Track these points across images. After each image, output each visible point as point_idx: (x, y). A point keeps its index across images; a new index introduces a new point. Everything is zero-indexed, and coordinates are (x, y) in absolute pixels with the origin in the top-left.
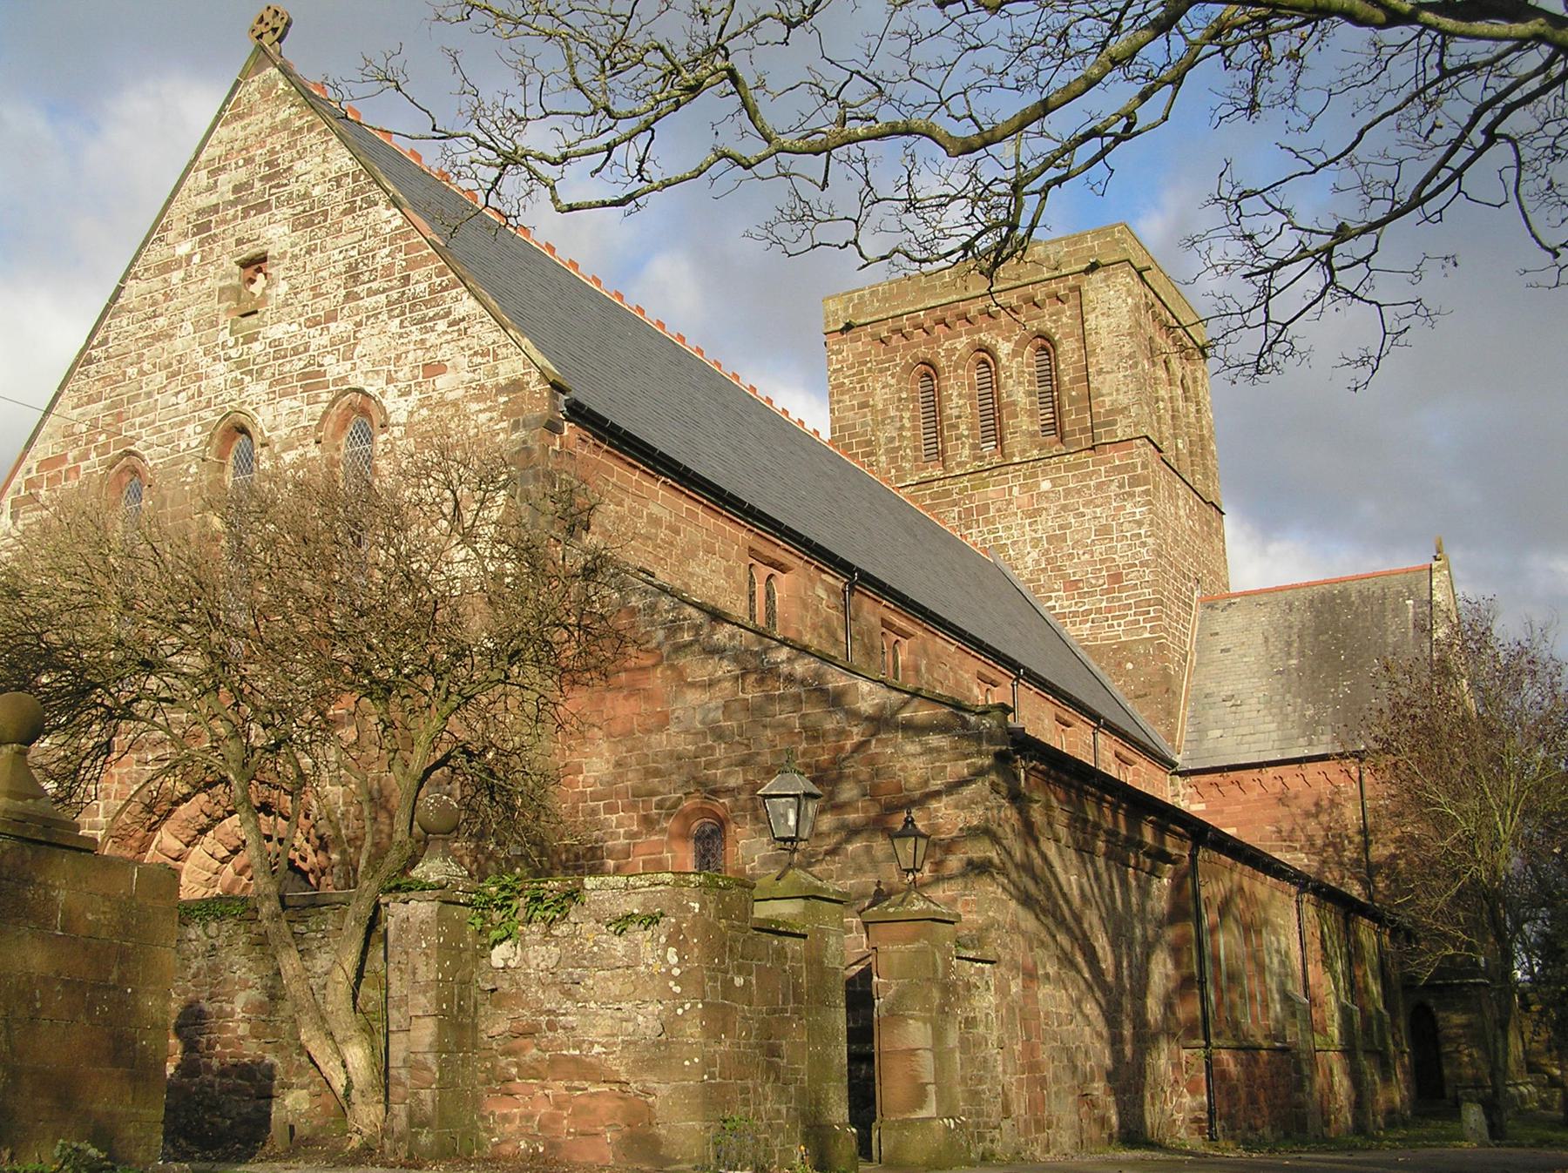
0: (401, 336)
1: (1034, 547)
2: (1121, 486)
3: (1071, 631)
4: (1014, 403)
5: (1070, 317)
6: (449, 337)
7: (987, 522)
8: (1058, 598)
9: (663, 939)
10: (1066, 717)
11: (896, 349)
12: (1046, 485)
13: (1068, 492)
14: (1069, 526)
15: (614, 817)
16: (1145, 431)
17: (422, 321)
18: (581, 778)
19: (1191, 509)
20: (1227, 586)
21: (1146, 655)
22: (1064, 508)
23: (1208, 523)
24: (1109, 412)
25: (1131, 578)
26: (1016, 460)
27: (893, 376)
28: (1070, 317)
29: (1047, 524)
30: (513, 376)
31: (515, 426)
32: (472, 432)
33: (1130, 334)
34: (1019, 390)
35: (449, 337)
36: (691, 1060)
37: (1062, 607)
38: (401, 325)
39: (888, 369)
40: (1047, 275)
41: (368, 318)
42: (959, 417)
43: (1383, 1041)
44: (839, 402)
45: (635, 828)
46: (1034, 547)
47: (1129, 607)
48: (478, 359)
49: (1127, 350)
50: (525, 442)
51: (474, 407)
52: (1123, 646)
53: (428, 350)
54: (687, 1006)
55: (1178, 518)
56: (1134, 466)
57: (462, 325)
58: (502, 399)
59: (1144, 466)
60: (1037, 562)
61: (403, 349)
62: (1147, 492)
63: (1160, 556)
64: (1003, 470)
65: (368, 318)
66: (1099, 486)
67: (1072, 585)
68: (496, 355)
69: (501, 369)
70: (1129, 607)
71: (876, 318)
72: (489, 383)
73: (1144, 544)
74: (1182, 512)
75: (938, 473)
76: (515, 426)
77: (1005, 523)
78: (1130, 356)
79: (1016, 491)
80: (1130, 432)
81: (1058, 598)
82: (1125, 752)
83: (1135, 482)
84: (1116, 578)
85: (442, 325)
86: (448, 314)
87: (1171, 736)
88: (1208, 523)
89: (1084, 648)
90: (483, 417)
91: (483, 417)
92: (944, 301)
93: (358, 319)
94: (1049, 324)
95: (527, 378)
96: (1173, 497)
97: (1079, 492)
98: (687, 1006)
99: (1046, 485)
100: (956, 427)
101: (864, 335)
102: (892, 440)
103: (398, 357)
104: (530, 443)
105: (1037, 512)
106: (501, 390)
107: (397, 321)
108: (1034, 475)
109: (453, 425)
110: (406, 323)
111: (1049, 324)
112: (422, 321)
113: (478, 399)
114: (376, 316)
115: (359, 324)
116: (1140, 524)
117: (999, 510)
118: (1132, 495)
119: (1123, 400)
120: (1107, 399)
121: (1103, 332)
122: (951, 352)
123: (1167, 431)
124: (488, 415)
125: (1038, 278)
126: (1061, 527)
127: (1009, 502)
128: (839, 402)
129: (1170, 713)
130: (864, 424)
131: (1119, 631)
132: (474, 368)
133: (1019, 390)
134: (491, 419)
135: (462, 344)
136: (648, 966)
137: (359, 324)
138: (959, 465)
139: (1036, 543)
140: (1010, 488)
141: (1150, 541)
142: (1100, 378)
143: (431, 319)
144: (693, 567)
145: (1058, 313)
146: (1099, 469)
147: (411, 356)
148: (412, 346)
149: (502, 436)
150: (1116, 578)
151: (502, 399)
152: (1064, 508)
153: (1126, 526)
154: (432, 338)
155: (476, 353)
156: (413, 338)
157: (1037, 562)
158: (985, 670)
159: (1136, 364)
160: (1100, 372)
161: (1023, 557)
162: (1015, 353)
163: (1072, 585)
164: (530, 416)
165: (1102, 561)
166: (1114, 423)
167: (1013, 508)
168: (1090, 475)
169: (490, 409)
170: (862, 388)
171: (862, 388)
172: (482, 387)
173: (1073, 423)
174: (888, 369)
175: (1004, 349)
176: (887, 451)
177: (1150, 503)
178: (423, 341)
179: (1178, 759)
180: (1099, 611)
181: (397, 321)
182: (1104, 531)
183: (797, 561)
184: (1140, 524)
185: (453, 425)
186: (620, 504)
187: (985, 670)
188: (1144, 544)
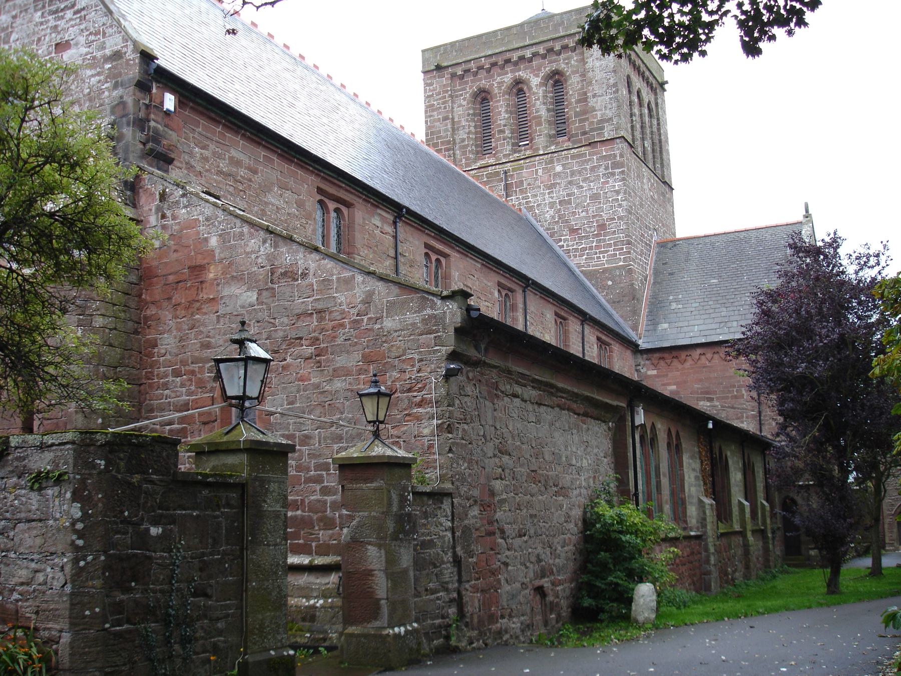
0: (42, 23)
1: (551, 208)
2: (607, 168)
3: (573, 263)
4: (540, 117)
5: (577, 61)
6: (73, 23)
7: (522, 191)
8: (565, 240)
9: (68, 495)
10: (563, 313)
11: (467, 83)
12: (559, 169)
13: (573, 173)
14: (573, 194)
15: (178, 379)
16: (622, 133)
17: (56, 12)
18: (156, 350)
19: (652, 185)
20: (674, 234)
21: (620, 276)
22: (570, 183)
23: (663, 195)
24: (602, 121)
25: (612, 227)
26: (541, 152)
27: (464, 99)
28: (577, 61)
29: (560, 193)
30: (115, 48)
31: (116, 86)
32: (87, 91)
33: (615, 71)
34: (539, 104)
35: (73, 23)
36: (91, 609)
37: (568, 246)
38: (43, 16)
39: (462, 95)
40: (562, 34)
41: (21, 12)
42: (505, 126)
43: (764, 523)
44: (431, 116)
45: (193, 388)
46: (551, 208)
47: (610, 245)
48: (92, 38)
49: (612, 81)
50: (121, 97)
51: (89, 72)
52: (605, 271)
53: (59, 33)
54: (90, 558)
55: (643, 190)
56: (615, 156)
57: (83, 13)
58: (108, 66)
59: (621, 156)
60: (553, 217)
61: (43, 33)
62: (623, 172)
63: (630, 213)
64: (532, 159)
65: (21, 12)
66: (593, 169)
67: (573, 231)
68: (104, 33)
69: (108, 45)
70: (610, 245)
71: (454, 62)
72: (99, 54)
73: (620, 206)
74: (646, 187)
75: (492, 161)
76: (116, 86)
77: (534, 192)
78: (615, 85)
79: (540, 171)
80: (613, 135)
81: (565, 240)
82: (604, 337)
83: (615, 165)
84: (602, 227)
85: (69, 14)
86: (73, 6)
87: (635, 328)
88: (663, 195)
89: (582, 272)
90: (94, 80)
91: (94, 80)
92: (497, 51)
93: (14, 13)
94: (563, 66)
95: (124, 50)
96: (640, 177)
97: (580, 172)
98: (90, 558)
99: (559, 169)
100: (503, 132)
101: (447, 74)
102: (463, 140)
103: (39, 40)
104: (125, 98)
105: (553, 186)
106: (107, 59)
107: (39, 13)
108: (551, 162)
109: (73, 87)
110: (46, 14)
111: (563, 66)
112: (56, 12)
113: (91, 66)
114: (26, 10)
115: (14, 17)
116: (618, 192)
117: (529, 184)
118: (613, 174)
119: (609, 114)
120: (599, 113)
121: (597, 71)
122: (501, 83)
123: (638, 135)
124: (97, 78)
125: (557, 35)
126: (568, 195)
127: (536, 179)
128: (431, 116)
129: (635, 312)
130: (446, 130)
131: (603, 261)
132: (89, 44)
133: (539, 104)
134: (99, 81)
135: (82, 27)
136: (56, 520)
137: (14, 17)
138: (505, 156)
139: (552, 205)
140: (537, 170)
141: (624, 203)
142: (595, 100)
143: (62, 10)
144: (270, 198)
145: (568, 58)
146: (593, 157)
147: (47, 39)
148: (49, 31)
149: (106, 93)
150: (602, 227)
151: (108, 66)
152: (570, 183)
153: (609, 195)
154: (62, 24)
155: (91, 34)
156: (50, 24)
157: (553, 217)
158: (503, 281)
159: (617, 91)
160: (594, 96)
161: (544, 214)
162: (541, 85)
163: (573, 231)
164: (126, 78)
165: (594, 217)
166: (602, 128)
167: (538, 183)
168: (587, 161)
169: (98, 74)
170: (445, 108)
171: (445, 108)
172: (94, 58)
173: (577, 129)
174: (462, 95)
175: (535, 81)
176: (461, 148)
177: (623, 179)
178: (56, 27)
179: (640, 342)
180: (591, 248)
181: (39, 13)
182: (595, 197)
183: (358, 199)
184: (618, 192)
185: (73, 87)
186: (204, 147)
187: (503, 281)
188: (620, 206)
